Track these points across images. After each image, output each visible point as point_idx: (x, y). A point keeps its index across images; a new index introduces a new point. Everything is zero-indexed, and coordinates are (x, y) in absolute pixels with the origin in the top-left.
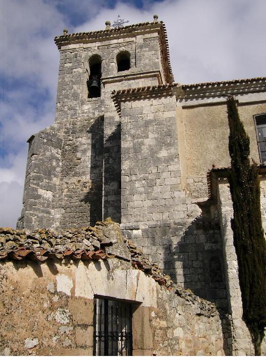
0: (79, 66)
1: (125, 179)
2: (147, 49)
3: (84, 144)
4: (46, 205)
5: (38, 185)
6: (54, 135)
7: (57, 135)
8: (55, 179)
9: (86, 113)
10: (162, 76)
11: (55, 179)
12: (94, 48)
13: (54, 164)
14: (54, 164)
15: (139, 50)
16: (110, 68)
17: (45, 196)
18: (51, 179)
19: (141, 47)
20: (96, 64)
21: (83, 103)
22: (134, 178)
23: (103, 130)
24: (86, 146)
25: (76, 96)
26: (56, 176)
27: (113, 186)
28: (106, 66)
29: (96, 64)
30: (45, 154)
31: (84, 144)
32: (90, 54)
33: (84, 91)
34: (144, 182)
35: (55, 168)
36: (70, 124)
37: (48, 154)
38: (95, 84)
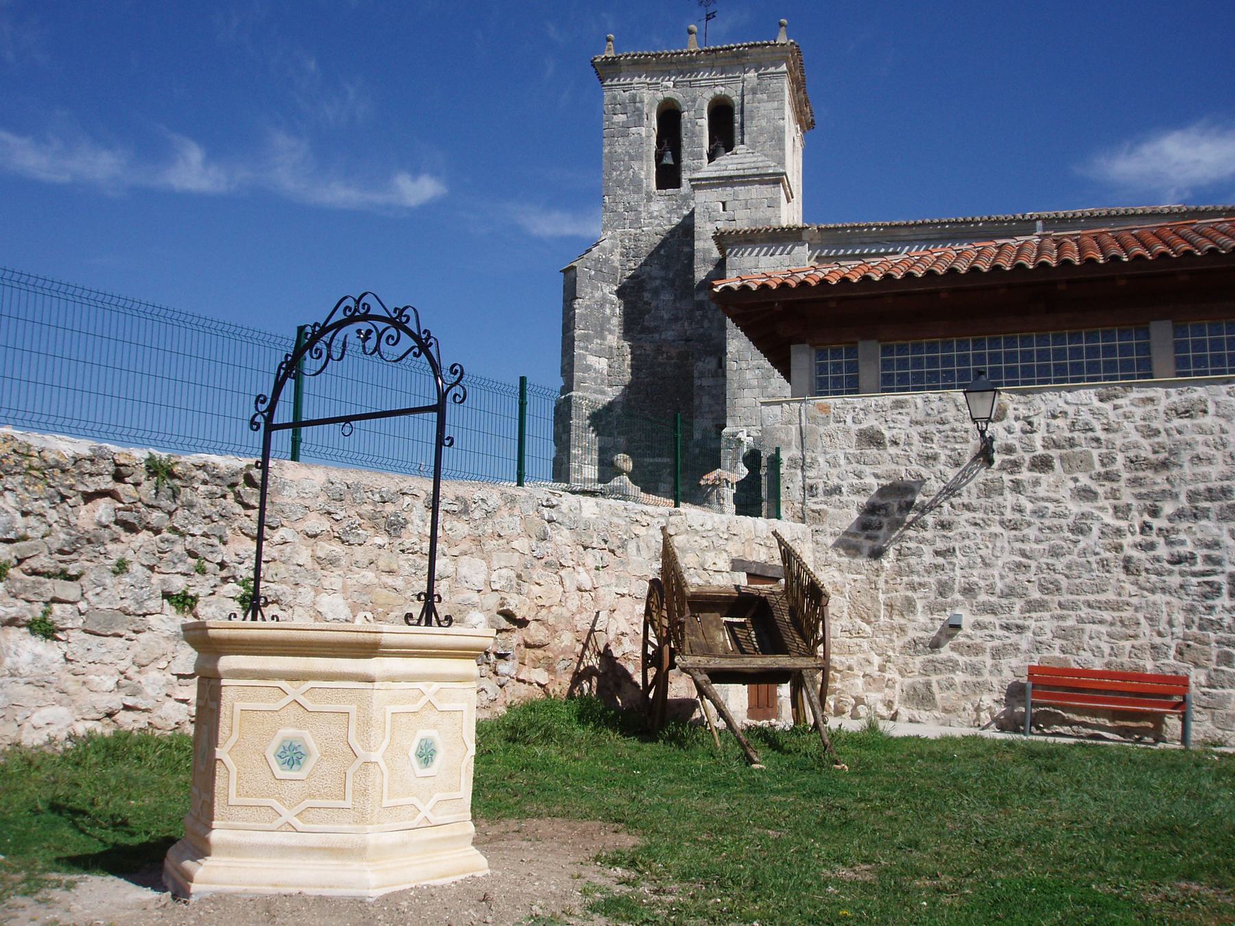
0: (639, 124)
1: (731, 365)
2: (765, 96)
3: (656, 278)
4: (599, 381)
5: (586, 349)
6: (606, 261)
7: (609, 260)
8: (610, 337)
9: (656, 218)
10: (1017, 736)
11: (610, 337)
12: (668, 88)
13: (608, 311)
14: (608, 311)
15: (750, 96)
16: (698, 127)
17: (597, 366)
18: (604, 338)
19: (754, 91)
20: (670, 118)
21: (649, 198)
22: (744, 365)
23: (693, 273)
24: (658, 282)
25: (637, 184)
26: (611, 332)
27: (712, 364)
28: (689, 125)
29: (670, 118)
30: (593, 297)
31: (656, 278)
32: (660, 96)
33: (648, 172)
34: (757, 371)
35: (609, 319)
36: (630, 239)
37: (598, 294)
38: (668, 160)
